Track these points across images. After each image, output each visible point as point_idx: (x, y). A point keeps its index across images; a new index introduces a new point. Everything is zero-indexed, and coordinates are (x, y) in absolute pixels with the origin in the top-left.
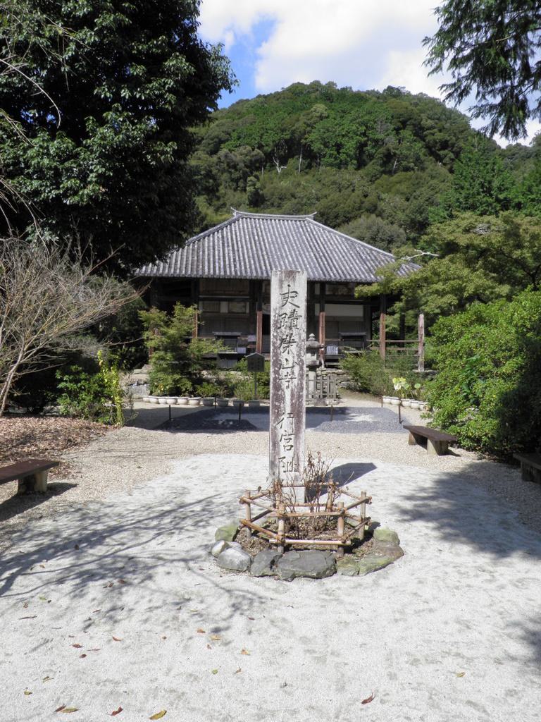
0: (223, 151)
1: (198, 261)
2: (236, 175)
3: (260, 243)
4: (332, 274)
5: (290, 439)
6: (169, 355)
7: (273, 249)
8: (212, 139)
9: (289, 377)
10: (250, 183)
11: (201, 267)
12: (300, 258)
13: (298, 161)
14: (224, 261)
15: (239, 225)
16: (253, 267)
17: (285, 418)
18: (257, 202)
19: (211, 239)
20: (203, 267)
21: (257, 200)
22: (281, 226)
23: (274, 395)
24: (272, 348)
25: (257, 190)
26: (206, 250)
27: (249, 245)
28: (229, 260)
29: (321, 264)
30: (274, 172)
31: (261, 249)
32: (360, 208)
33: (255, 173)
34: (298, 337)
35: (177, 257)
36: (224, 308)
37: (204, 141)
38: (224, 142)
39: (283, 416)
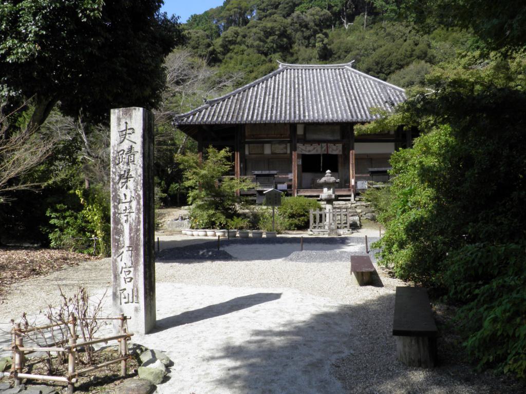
0: (297, 12)
1: (240, 109)
2: (307, 33)
3: (299, 91)
4: (359, 115)
5: (130, 271)
6: (203, 193)
7: (309, 95)
8: (287, 4)
9: (128, 211)
10: (319, 39)
11: (241, 114)
12: (332, 102)
13: (364, 18)
14: (263, 108)
15: (283, 75)
16: (288, 112)
17: (125, 252)
18: (326, 56)
19: (256, 89)
20: (243, 114)
21: (326, 55)
22: (321, 75)
23: (115, 228)
24: (111, 183)
25: (325, 45)
26: (249, 99)
27: (288, 93)
28: (268, 107)
29: (351, 106)
30: (343, 28)
31: (299, 96)
32: (411, 56)
33: (324, 31)
34: (134, 172)
35: (222, 106)
36: (267, 150)
37: (280, 6)
38: (298, 5)
39: (123, 250)
